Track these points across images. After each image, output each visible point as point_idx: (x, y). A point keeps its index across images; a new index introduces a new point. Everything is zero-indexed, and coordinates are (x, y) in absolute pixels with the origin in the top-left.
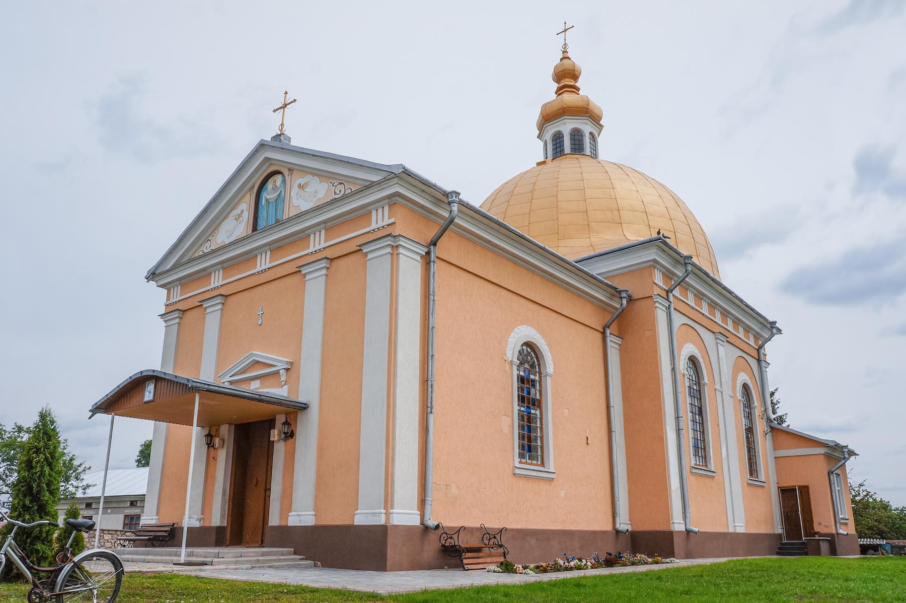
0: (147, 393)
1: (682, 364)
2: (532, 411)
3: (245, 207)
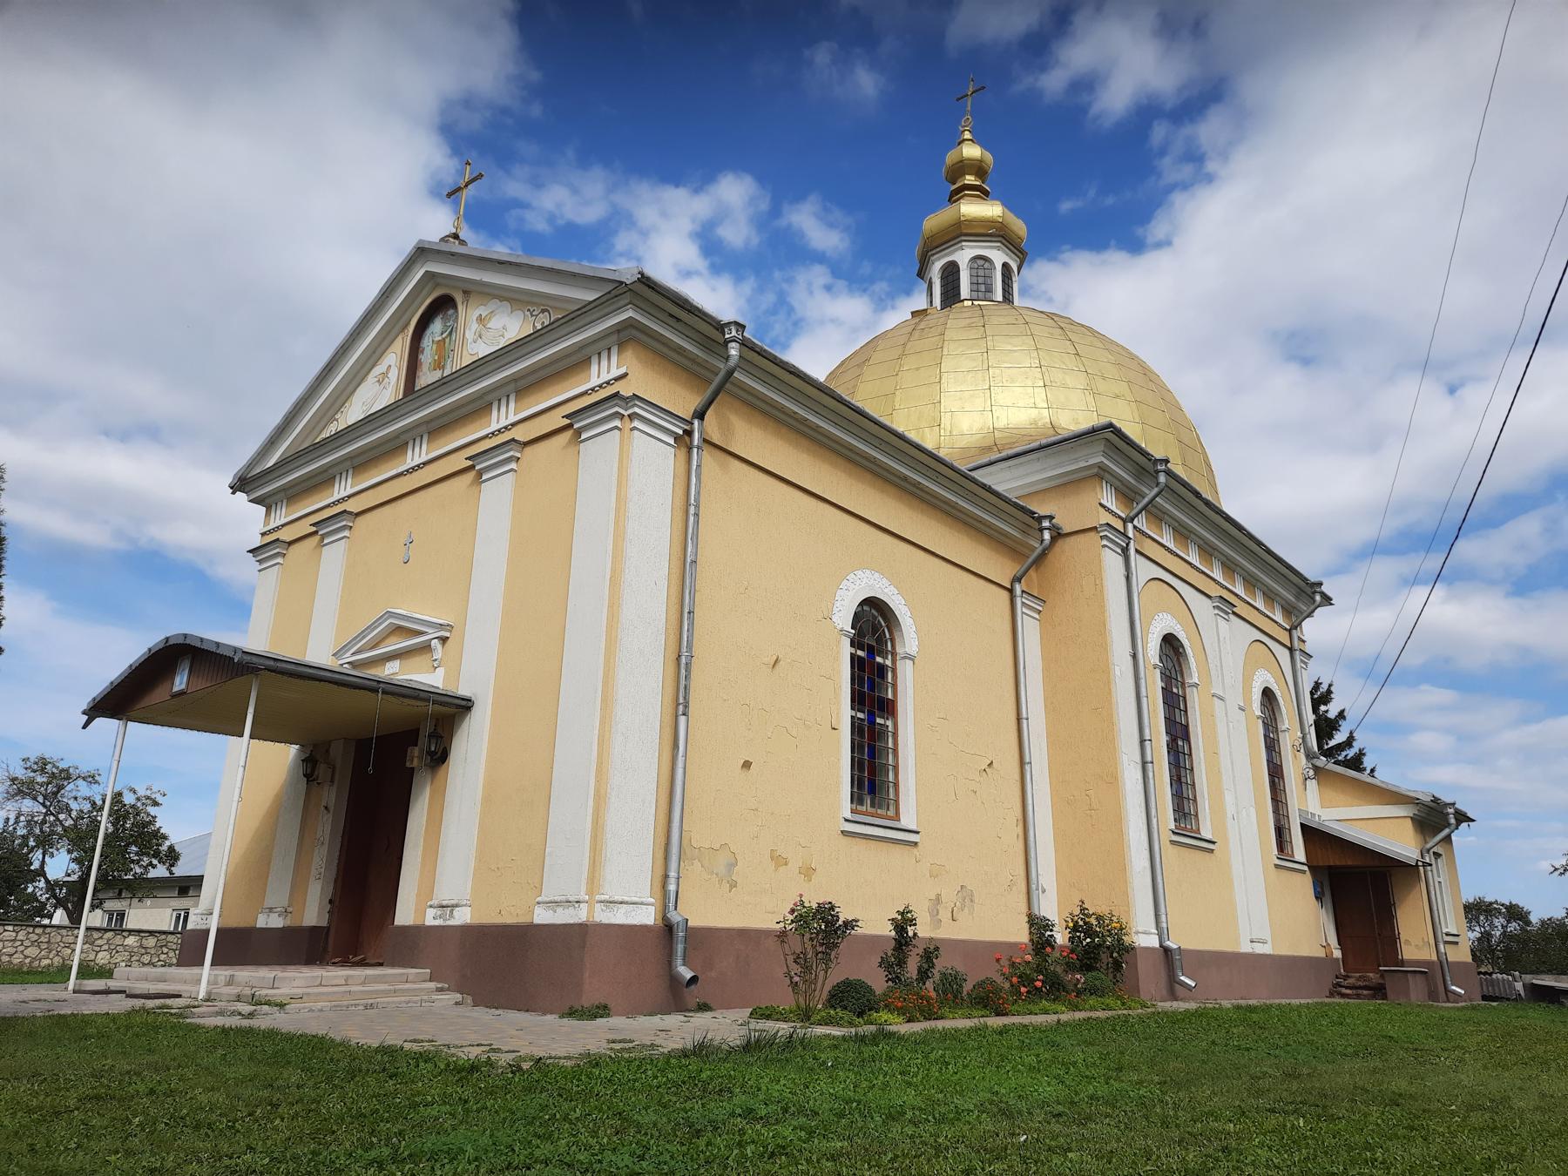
0: (177, 680)
1: (1152, 650)
2: (879, 720)
3: (394, 360)
